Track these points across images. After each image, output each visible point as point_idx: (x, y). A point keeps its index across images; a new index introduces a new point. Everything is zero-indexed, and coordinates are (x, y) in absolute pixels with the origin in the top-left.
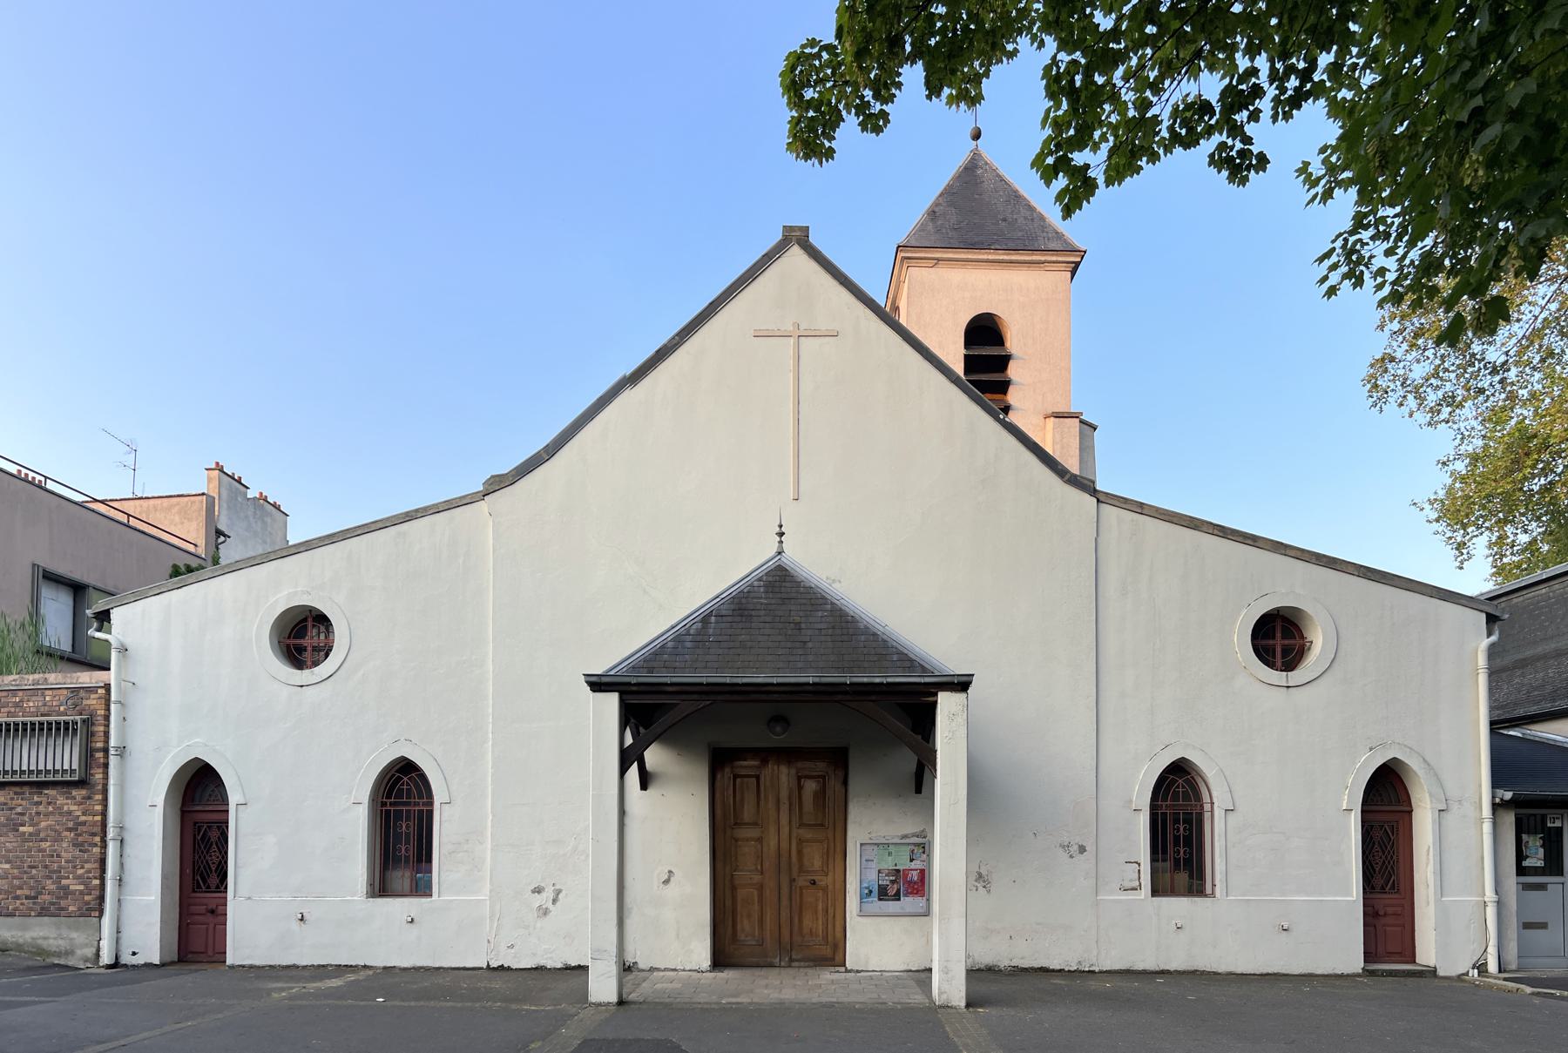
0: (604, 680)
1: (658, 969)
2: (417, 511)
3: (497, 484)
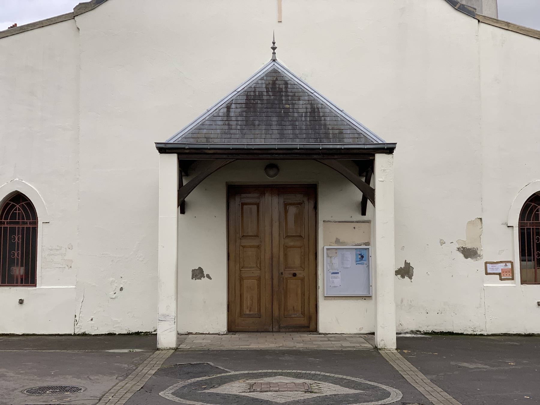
0: (168, 146)
1: (191, 333)
2: (28, 25)
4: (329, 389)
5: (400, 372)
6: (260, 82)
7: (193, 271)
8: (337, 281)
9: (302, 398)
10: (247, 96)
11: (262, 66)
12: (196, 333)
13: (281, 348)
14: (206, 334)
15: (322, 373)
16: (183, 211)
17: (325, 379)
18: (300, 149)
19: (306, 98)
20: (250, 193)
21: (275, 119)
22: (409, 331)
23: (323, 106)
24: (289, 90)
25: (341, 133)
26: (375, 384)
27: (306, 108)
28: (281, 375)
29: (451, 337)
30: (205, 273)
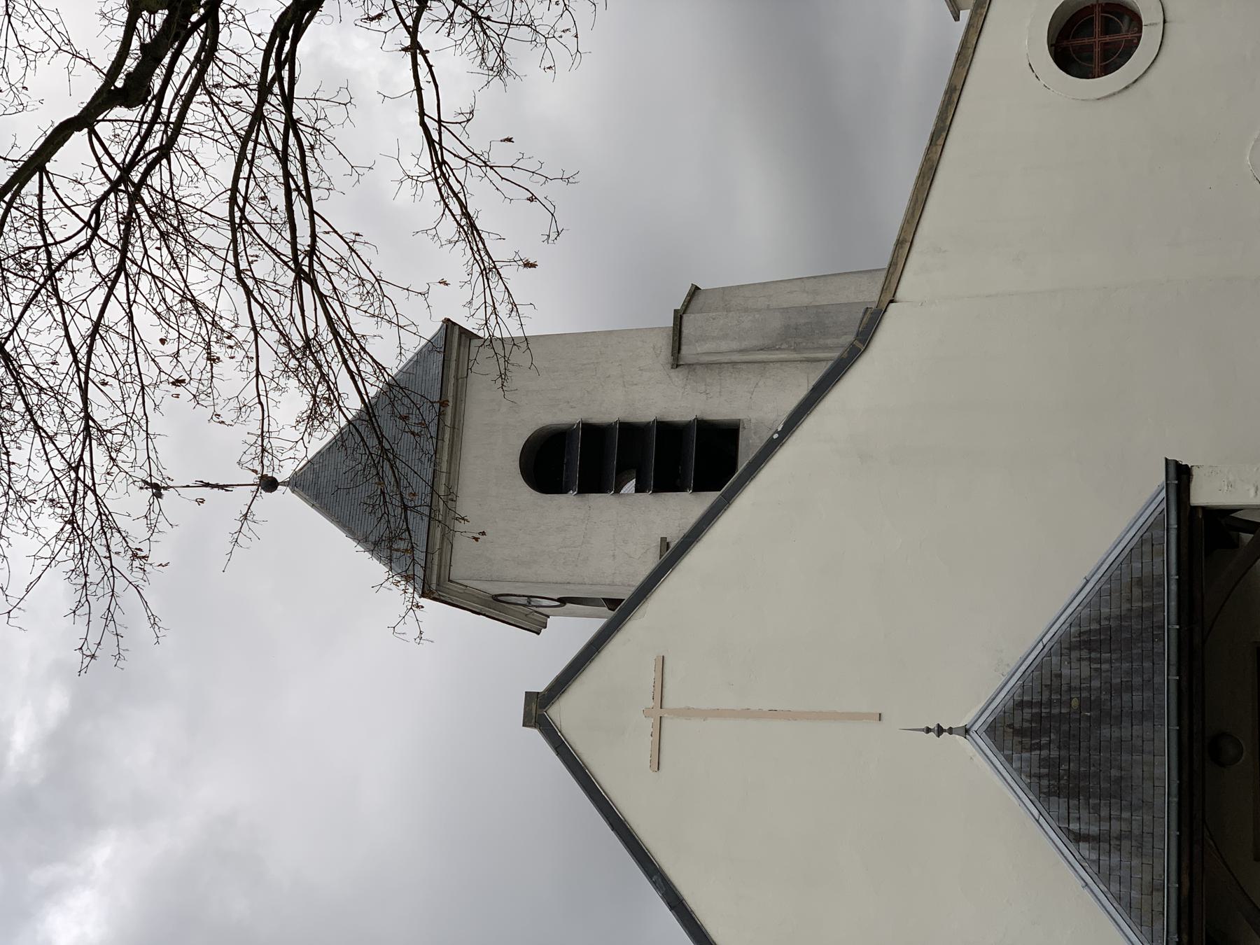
19: (1055, 660)
21: (1106, 731)
23: (1076, 621)
25: (1140, 582)
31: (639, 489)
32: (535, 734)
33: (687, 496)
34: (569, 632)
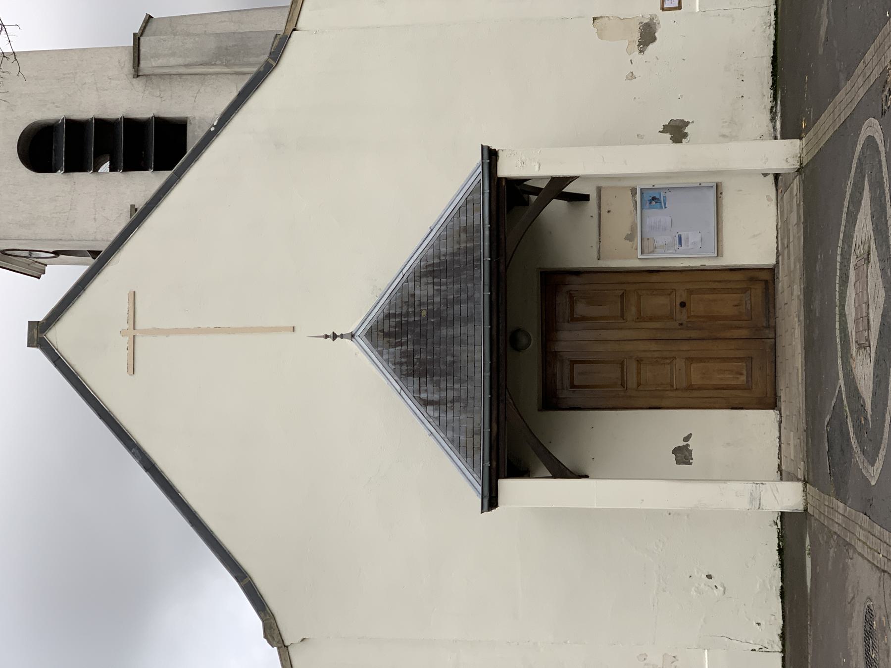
0: (486, 492)
1: (779, 466)
3: (272, 632)
4: (864, 228)
5: (836, 128)
6: (386, 357)
7: (678, 462)
8: (693, 237)
9: (878, 264)
10: (407, 375)
11: (362, 355)
12: (780, 458)
13: (802, 318)
14: (780, 442)
15: (840, 244)
16: (587, 477)
17: (849, 237)
18: (490, 291)
19: (411, 284)
20: (555, 375)
21: (444, 332)
22: (771, 125)
23: (424, 258)
24: (399, 311)
25: (466, 230)
26: (855, 161)
27: (427, 284)
28: (844, 306)
29: (779, 60)
30: (682, 443)
31: (113, 169)
32: (37, 352)
33: (149, 174)
34: (62, 276)
